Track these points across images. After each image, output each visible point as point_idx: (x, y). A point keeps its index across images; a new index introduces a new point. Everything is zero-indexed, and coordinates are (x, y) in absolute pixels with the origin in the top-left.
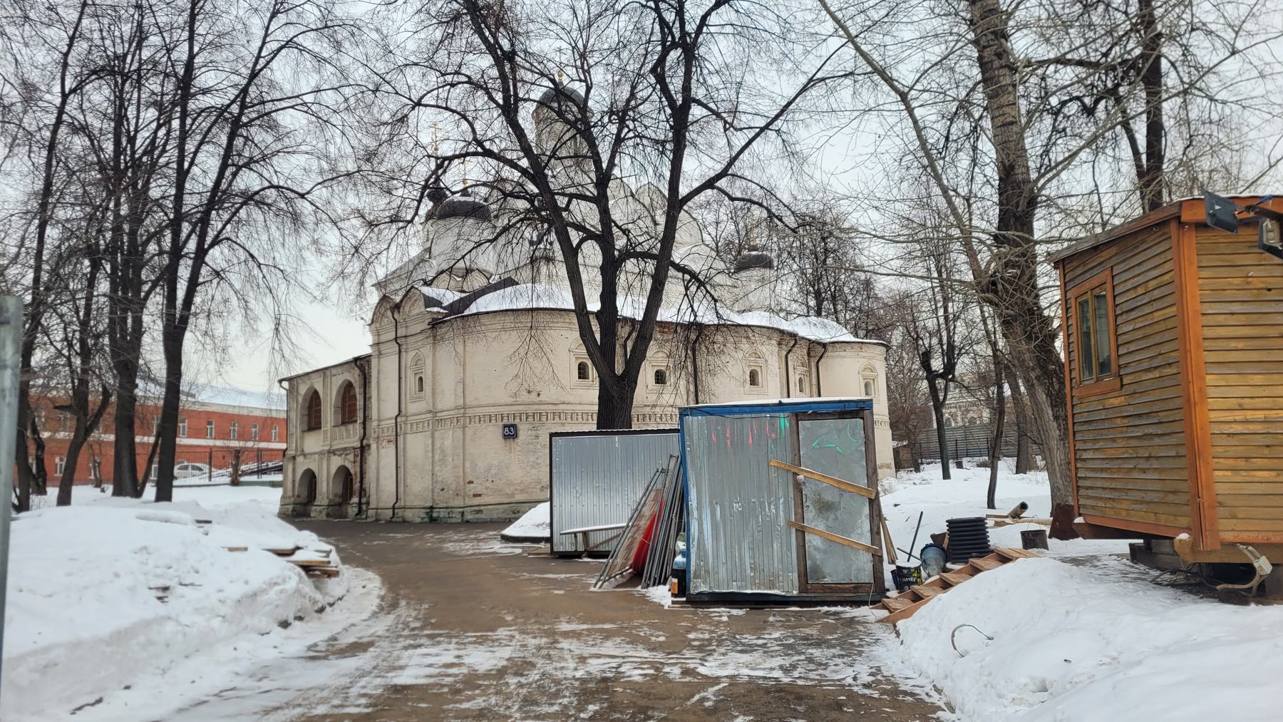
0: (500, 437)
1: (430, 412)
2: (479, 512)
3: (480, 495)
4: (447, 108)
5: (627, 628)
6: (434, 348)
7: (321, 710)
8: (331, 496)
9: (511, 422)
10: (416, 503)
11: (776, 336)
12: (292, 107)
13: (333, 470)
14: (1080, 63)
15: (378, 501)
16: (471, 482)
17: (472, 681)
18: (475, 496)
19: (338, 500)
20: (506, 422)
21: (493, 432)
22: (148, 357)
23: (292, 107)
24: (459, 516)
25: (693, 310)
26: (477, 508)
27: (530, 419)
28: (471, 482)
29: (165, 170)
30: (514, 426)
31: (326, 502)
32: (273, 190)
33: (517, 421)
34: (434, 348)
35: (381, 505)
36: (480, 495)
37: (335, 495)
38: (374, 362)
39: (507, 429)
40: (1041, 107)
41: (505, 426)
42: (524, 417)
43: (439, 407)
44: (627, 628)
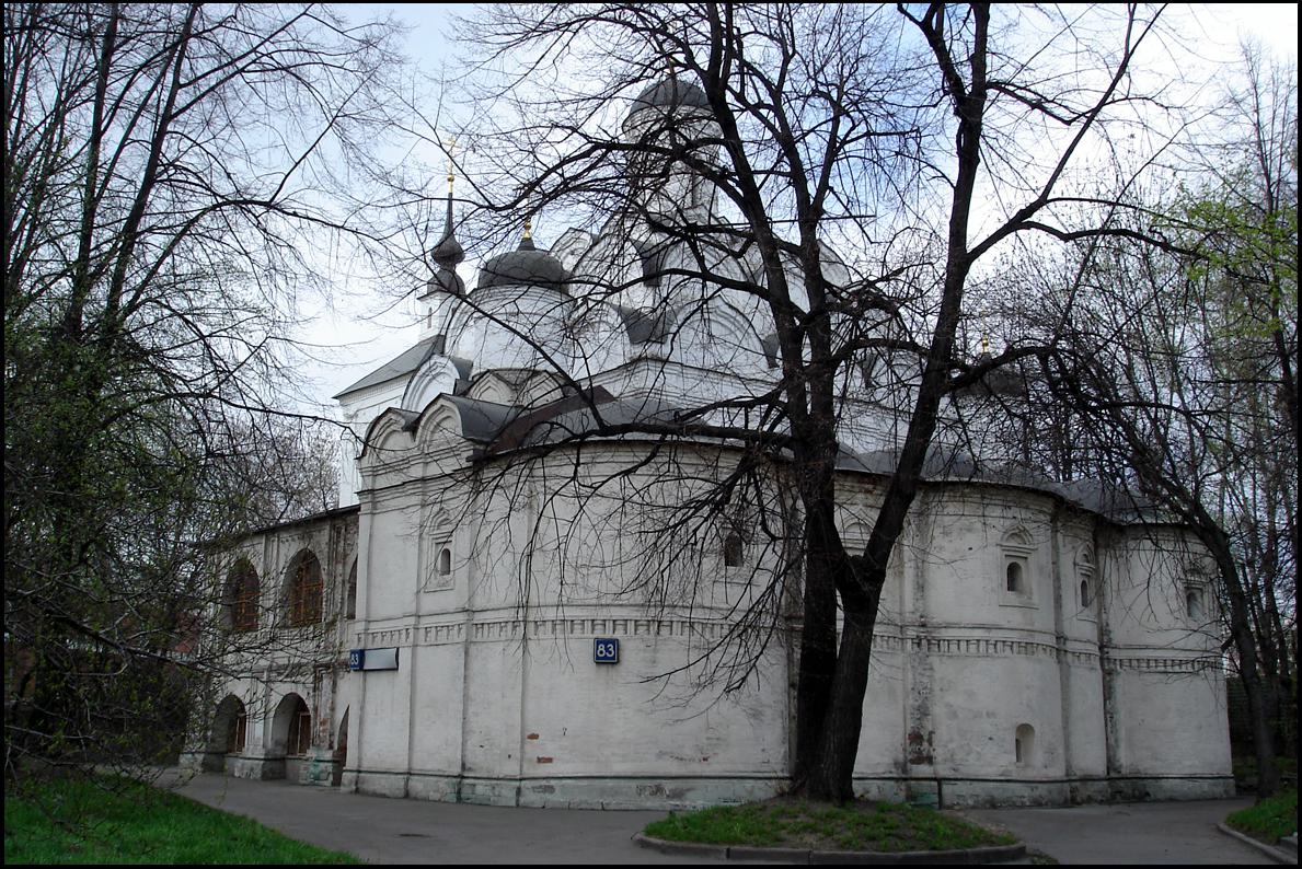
0: (591, 659)
1: (465, 611)
2: (550, 789)
3: (550, 760)
4: (283, 29)
5: (755, 479)
8: (270, 744)
9: (608, 635)
10: (430, 766)
11: (1049, 507)
13: (276, 699)
15: (360, 759)
16: (534, 736)
18: (540, 760)
19: (280, 752)
20: (599, 634)
25: (277, 69)
26: (544, 783)
27: (642, 630)
28: (534, 736)
29: (1224, 437)
30: (615, 642)
31: (260, 753)
33: (619, 634)
35: (366, 765)
36: (550, 760)
37: (277, 743)
38: (364, 521)
39: (602, 647)
41: (599, 642)
42: (631, 626)
43: (479, 603)
44: (755, 479)
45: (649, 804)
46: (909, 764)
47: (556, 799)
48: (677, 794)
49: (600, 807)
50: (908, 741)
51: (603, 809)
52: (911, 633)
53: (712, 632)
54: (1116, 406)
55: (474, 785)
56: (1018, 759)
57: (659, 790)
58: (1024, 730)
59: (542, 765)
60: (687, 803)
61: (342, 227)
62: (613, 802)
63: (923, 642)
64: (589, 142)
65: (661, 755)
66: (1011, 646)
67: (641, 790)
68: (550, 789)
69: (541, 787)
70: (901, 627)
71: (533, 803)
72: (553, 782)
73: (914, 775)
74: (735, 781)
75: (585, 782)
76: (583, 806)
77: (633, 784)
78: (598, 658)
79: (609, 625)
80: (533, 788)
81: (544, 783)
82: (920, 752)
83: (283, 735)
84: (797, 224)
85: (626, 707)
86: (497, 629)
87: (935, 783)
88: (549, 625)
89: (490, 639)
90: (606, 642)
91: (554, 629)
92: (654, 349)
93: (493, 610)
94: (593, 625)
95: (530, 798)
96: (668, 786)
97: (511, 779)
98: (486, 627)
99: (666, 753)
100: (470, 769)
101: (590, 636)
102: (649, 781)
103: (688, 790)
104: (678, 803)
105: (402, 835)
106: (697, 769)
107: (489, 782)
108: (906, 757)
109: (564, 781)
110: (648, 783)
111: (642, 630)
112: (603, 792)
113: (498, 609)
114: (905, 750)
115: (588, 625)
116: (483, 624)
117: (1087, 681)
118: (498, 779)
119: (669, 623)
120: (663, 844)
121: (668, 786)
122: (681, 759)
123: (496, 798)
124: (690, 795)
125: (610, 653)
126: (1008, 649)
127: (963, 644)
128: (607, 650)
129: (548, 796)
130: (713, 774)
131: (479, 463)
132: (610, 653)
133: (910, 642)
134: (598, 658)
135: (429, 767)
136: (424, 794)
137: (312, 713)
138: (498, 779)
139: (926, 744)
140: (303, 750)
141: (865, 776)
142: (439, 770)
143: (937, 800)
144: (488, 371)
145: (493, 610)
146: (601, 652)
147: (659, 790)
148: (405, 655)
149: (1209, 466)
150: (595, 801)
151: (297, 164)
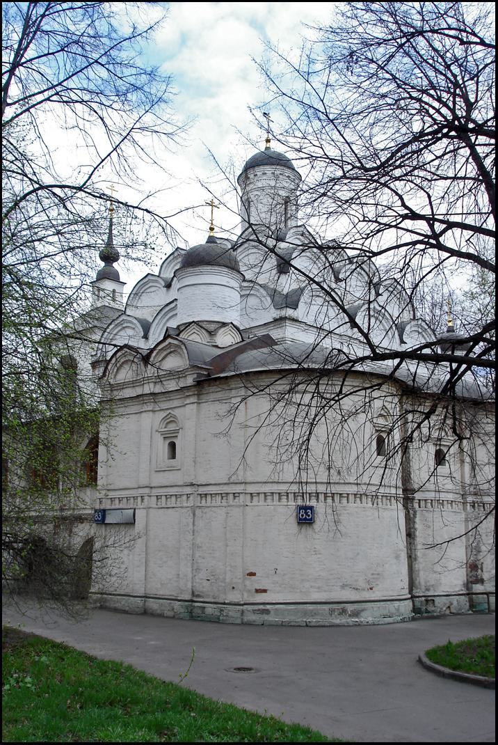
2: (267, 612)
3: (265, 591)
6: (198, 411)
7: (66, 5)
12: (48, 99)
14: (418, 284)
17: (402, 476)
18: (257, 591)
20: (300, 502)
21: (286, 511)
22: (359, 284)
23: (48, 99)
24: (239, 615)
26: (261, 607)
27: (329, 500)
30: (311, 508)
32: (357, 320)
33: (313, 503)
34: (198, 411)
36: (265, 591)
39: (302, 512)
40: (445, 131)
41: (301, 508)
45: (337, 621)
46: (470, 585)
47: (271, 619)
48: (356, 614)
49: (305, 624)
50: (469, 569)
51: (307, 626)
52: (470, 499)
53: (361, 500)
55: (204, 607)
57: (344, 611)
59: (259, 594)
60: (362, 620)
61: (137, 207)
62: (313, 620)
63: (476, 504)
64: (435, 124)
65: (343, 587)
66: (348, 498)
67: (332, 612)
68: (267, 612)
69: (259, 610)
70: (463, 495)
71: (254, 621)
72: (268, 607)
73: (474, 591)
74: (389, 603)
75: (292, 607)
76: (292, 624)
77: (326, 607)
78: (300, 519)
80: (253, 610)
81: (261, 607)
82: (477, 576)
84: (491, 216)
85: (320, 554)
86: (219, 498)
87: (485, 596)
89: (213, 504)
91: (265, 499)
92: (289, 312)
93: (215, 484)
94: (265, 496)
96: (350, 608)
97: (235, 605)
98: (209, 497)
99: (347, 586)
100: (198, 596)
102: (336, 605)
103: (363, 610)
104: (357, 620)
105: (239, 669)
106: (367, 595)
107: (215, 606)
108: (467, 580)
109: (277, 606)
110: (335, 606)
111: (329, 500)
112: (305, 613)
113: (219, 484)
114: (467, 575)
116: (227, 494)
118: (224, 604)
119: (346, 495)
120: (486, 681)
121: (350, 608)
122: (357, 589)
123: (225, 618)
124: (363, 614)
125: (309, 516)
127: (423, 503)
128: (306, 513)
129: (266, 617)
130: (376, 599)
131: (199, 384)
132: (309, 516)
133: (468, 505)
134: (300, 519)
135: (161, 593)
136: (159, 612)
138: (224, 604)
139: (480, 571)
141: (449, 593)
142: (163, 595)
143: (487, 607)
144: (193, 322)
145: (215, 484)
146: (302, 516)
147: (344, 611)
148: (140, 515)
150: (300, 620)
151: (103, 160)
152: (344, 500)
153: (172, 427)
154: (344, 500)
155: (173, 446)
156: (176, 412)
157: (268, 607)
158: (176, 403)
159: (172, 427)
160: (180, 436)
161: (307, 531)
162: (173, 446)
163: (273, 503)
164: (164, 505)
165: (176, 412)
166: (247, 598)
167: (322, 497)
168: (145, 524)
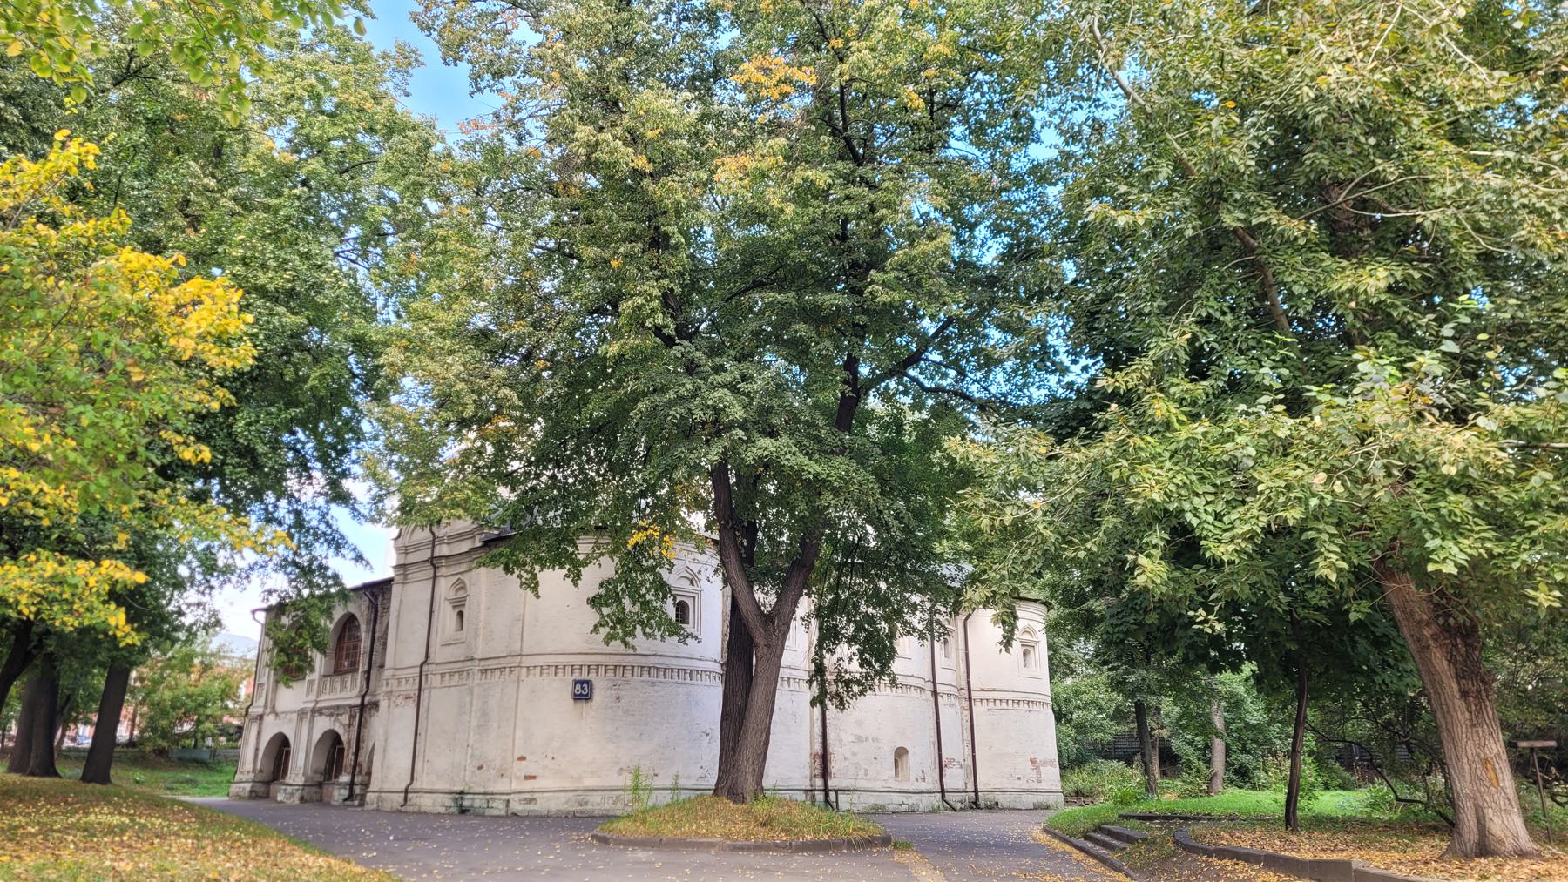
3: (534, 777)
9: (585, 677)
20: (577, 676)
21: (562, 688)
27: (610, 674)
30: (589, 683)
31: (300, 780)
33: (592, 676)
36: (534, 777)
37: (315, 772)
41: (576, 682)
42: (602, 670)
54: (1411, 308)
56: (896, 774)
58: (900, 753)
79: (585, 669)
83: (322, 765)
88: (538, 669)
90: (582, 682)
95: (516, 806)
101: (570, 679)
111: (610, 674)
115: (568, 669)
117: (952, 715)
126: (646, 674)
127: (681, 673)
137: (346, 746)
140: (336, 777)
142: (724, 616)
149: (680, 21)
152: (628, 674)
153: (461, 594)
154: (628, 674)
155: (461, 614)
156: (465, 578)
157: (536, 795)
158: (464, 567)
159: (461, 594)
160: (467, 603)
161: (582, 704)
162: (461, 614)
163: (792, 665)
164: (447, 684)
165: (465, 578)
166: (515, 786)
167: (602, 670)
168: (521, 687)
